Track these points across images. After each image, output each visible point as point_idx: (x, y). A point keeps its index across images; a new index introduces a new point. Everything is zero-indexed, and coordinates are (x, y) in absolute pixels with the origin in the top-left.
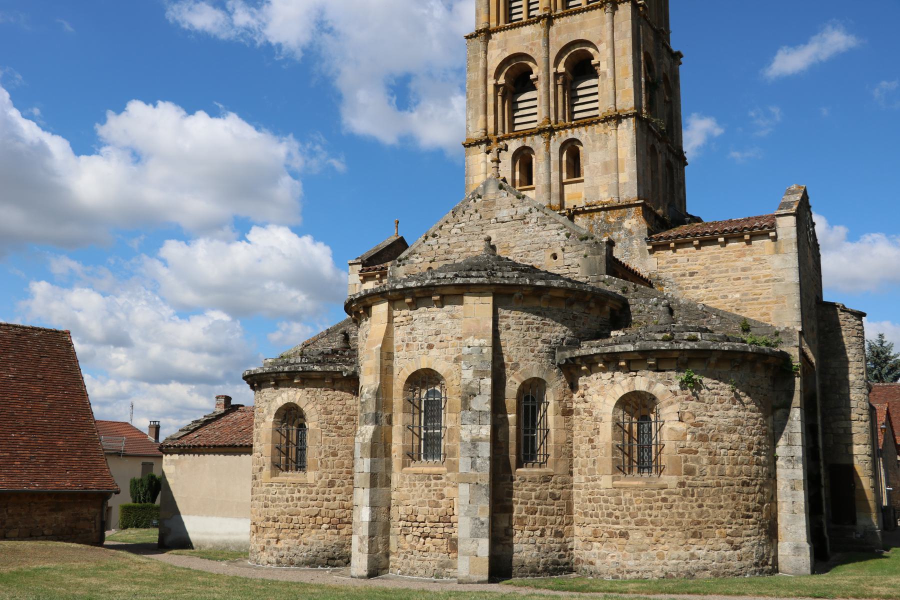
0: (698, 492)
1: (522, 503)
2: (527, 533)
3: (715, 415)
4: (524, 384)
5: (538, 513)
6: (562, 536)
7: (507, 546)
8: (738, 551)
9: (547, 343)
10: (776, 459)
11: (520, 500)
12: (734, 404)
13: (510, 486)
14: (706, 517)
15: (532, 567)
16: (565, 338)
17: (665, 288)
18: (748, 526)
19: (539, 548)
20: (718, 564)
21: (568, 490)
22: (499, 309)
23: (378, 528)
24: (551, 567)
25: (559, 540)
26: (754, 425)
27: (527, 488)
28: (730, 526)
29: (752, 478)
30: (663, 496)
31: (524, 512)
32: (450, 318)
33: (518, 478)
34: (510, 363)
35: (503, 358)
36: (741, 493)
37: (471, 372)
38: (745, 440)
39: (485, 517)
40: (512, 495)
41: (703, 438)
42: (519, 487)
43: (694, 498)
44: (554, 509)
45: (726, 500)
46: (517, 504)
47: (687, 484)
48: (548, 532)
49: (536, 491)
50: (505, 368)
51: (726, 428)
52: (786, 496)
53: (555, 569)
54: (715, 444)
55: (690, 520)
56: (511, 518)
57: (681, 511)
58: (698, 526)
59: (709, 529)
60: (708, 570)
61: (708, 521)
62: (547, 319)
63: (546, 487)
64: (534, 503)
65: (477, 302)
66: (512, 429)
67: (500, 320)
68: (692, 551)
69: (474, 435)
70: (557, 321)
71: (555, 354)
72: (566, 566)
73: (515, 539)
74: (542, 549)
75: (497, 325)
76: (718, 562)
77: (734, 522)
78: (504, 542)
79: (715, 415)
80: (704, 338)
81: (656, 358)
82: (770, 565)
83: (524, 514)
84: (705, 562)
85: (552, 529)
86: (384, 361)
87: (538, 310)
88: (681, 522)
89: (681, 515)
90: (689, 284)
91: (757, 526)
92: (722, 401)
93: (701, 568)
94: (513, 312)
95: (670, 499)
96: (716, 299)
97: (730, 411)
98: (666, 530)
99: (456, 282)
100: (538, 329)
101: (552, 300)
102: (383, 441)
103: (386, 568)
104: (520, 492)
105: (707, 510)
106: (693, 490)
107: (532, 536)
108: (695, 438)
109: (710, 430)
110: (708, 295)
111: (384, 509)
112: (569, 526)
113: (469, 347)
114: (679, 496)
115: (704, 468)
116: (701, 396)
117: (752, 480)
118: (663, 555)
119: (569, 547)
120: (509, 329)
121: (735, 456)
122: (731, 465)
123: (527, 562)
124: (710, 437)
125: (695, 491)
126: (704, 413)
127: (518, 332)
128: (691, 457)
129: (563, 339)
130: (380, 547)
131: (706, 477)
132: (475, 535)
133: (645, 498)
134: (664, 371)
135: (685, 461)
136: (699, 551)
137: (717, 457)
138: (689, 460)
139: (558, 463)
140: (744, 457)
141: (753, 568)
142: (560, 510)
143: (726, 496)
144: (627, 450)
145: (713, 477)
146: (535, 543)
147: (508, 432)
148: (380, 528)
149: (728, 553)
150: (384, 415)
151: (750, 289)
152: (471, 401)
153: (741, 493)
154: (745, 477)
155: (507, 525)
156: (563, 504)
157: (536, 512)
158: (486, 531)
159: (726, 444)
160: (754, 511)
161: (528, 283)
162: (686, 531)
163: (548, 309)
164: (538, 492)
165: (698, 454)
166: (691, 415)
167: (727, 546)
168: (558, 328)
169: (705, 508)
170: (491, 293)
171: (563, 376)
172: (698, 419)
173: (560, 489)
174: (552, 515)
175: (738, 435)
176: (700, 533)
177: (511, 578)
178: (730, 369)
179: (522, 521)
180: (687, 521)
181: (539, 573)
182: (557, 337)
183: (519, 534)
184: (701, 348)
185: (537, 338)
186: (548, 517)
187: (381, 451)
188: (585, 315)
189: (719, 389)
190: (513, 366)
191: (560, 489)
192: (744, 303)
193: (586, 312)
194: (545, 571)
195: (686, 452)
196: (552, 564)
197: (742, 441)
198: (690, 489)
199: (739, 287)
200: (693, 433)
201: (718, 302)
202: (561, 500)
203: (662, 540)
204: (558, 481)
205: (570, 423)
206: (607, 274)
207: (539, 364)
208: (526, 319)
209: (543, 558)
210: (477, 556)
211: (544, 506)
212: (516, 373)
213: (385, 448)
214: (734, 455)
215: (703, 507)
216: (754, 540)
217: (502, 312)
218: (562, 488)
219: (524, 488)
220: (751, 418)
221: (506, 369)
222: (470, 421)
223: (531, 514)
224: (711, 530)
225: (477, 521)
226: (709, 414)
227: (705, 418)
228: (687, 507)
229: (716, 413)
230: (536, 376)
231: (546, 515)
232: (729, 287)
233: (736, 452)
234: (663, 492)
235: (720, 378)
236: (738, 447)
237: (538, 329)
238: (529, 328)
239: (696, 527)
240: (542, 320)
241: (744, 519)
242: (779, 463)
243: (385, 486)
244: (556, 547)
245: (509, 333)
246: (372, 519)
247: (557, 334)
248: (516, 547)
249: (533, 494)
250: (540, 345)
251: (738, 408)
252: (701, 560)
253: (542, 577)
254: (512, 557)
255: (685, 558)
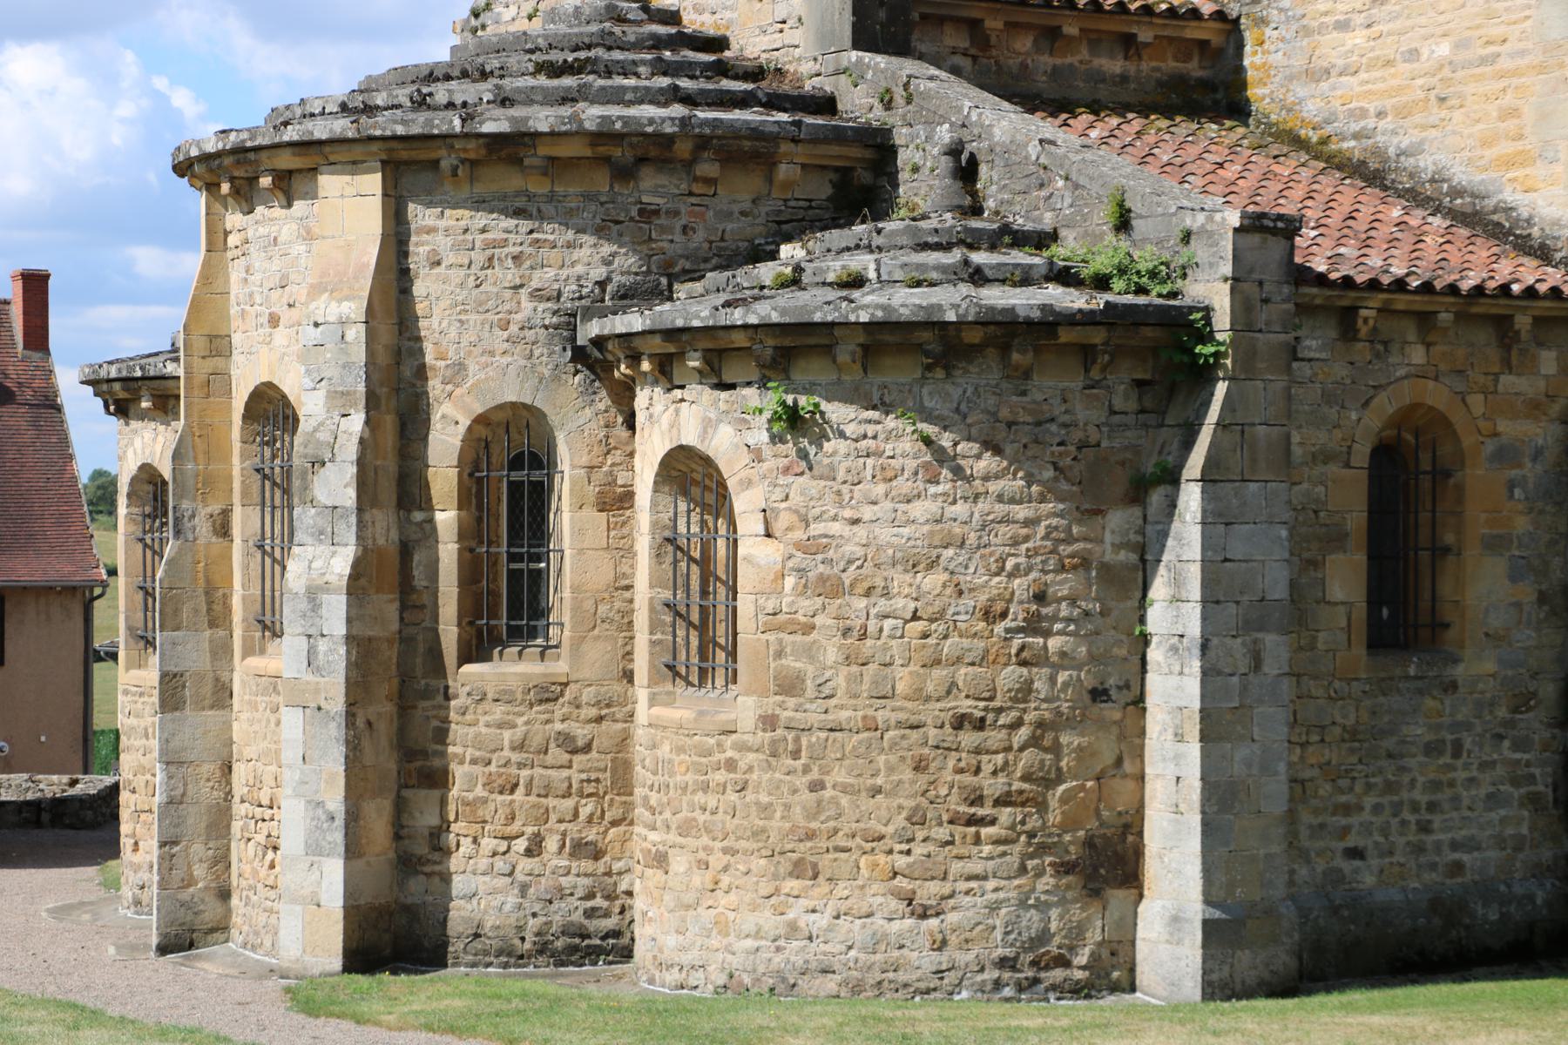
0: (810, 746)
1: (474, 762)
2: (488, 844)
3: (866, 517)
4: (481, 420)
5: (521, 790)
6: (597, 855)
7: (436, 879)
8: (933, 922)
9: (548, 300)
10: (1145, 640)
11: (470, 753)
12: (934, 481)
13: (442, 713)
14: (828, 819)
15: (503, 938)
16: (608, 279)
17: (1268, 32)
18: (975, 850)
19: (524, 889)
20: (862, 956)
21: (620, 726)
22: (411, 206)
23: (190, 821)
24: (559, 944)
25: (587, 865)
26: (1015, 542)
27: (487, 718)
28: (905, 847)
29: (997, 704)
30: (729, 754)
31: (480, 786)
32: (305, 240)
33: (463, 691)
34: (442, 364)
35: (421, 352)
36: (948, 749)
37: (321, 394)
38: (971, 590)
39: (335, 801)
40: (446, 736)
41: (830, 588)
42: (469, 717)
43: (799, 764)
44: (569, 778)
45: (891, 769)
46: (462, 762)
47: (782, 723)
48: (551, 844)
49: (514, 726)
50: (427, 379)
51: (899, 555)
52: (1164, 760)
53: (573, 949)
54: (861, 603)
55: (788, 825)
56: (443, 802)
57: (764, 799)
58: (809, 844)
59: (838, 855)
60: (834, 972)
61: (836, 831)
62: (548, 227)
63: (546, 716)
64: (507, 763)
65: (350, 191)
66: (448, 552)
67: (414, 239)
68: (791, 915)
69: (314, 574)
70: (580, 231)
71: (575, 330)
72: (611, 941)
73: (455, 863)
74: (532, 890)
75: (406, 254)
76: (863, 949)
77: (920, 835)
78: (427, 869)
79: (866, 517)
80: (884, 277)
81: (704, 350)
82: (1083, 968)
83: (479, 791)
84: (827, 948)
85: (564, 834)
86: (196, 360)
87: (520, 202)
88: (764, 830)
89: (766, 810)
90: (1326, 13)
91: (1017, 849)
92: (890, 474)
93: (813, 965)
94: (448, 212)
95: (742, 765)
96: (1389, 63)
97: (917, 504)
98: (734, 852)
99: (286, 138)
100: (516, 258)
101: (555, 167)
102: (202, 582)
103: (221, 928)
104: (472, 730)
105: (832, 798)
106: (797, 740)
107: (504, 853)
108: (805, 586)
109: (850, 562)
110: (1373, 49)
111: (210, 768)
112: (622, 828)
113: (316, 325)
114: (761, 756)
115: (828, 674)
116: (826, 461)
117: (1000, 710)
118: (727, 922)
119: (623, 887)
120: (438, 263)
121: (931, 641)
122: (912, 668)
123: (489, 924)
124: (847, 583)
125: (804, 742)
126: (832, 513)
127: (462, 272)
128: (794, 643)
129: (602, 284)
130: (199, 871)
131: (833, 702)
132: (315, 849)
133: (696, 759)
134: (732, 387)
135: (779, 654)
136: (813, 917)
137: (869, 642)
138: (788, 650)
139: (585, 647)
140: (966, 642)
141: (991, 974)
142: (589, 781)
143: (893, 758)
144: (695, 617)
145: (853, 702)
146: (511, 874)
147: (437, 560)
148: (195, 819)
149: (896, 926)
150: (203, 512)
151: (1478, 22)
152: (315, 478)
153: (948, 749)
154: (970, 702)
155: (434, 821)
156: (602, 765)
157: (516, 785)
158: (338, 837)
159: (899, 603)
160: (998, 803)
161: (458, 129)
162: (777, 858)
163: (551, 198)
164: (519, 732)
165: (814, 635)
166: (795, 518)
167: (895, 905)
168: (583, 253)
169: (828, 793)
170: (379, 164)
171: (604, 393)
172: (817, 529)
173: (590, 721)
174: (564, 797)
175: (946, 576)
176: (814, 866)
177: (445, 966)
178: (918, 374)
179: (473, 812)
180: (780, 829)
181: (521, 957)
182: (579, 278)
183: (466, 846)
184: (787, 320)
185: (516, 288)
186: (551, 802)
187: (196, 611)
188: (693, 200)
189: (881, 437)
190: (449, 373)
191: (590, 721)
192: (1460, 74)
193: (696, 191)
194: (541, 952)
195: (779, 628)
196: (563, 933)
197: (961, 593)
198: (790, 736)
199: (1447, 17)
200: (801, 571)
201: (1393, 76)
202: (594, 754)
203: (726, 880)
204: (584, 699)
205: (625, 531)
206: (857, 45)
207: (523, 362)
208: (483, 231)
209: (534, 915)
210: (319, 906)
211: (538, 771)
212: (458, 392)
213: (210, 603)
214: (925, 636)
215: (823, 787)
216: (996, 890)
217: (420, 216)
218: (599, 719)
219: (483, 719)
220: (1006, 520)
221: (431, 383)
222: (312, 535)
223: (501, 793)
224: (843, 855)
225: (320, 811)
226: (848, 513)
227: (836, 528)
228: (778, 788)
229: (867, 513)
230: (514, 399)
231: (546, 796)
232: (1423, 20)
233: (934, 626)
234: (729, 741)
235: (884, 404)
236: (943, 612)
237: (516, 258)
238: (491, 259)
239: (802, 847)
240: (531, 232)
241: (960, 829)
242: (1154, 654)
243: (212, 707)
244: (575, 887)
245: (438, 275)
246: (169, 796)
247: (580, 269)
248: (459, 884)
249: (507, 735)
250: (527, 305)
251: (944, 494)
252: (816, 942)
253: (531, 969)
254: (448, 911)
255: (772, 934)
